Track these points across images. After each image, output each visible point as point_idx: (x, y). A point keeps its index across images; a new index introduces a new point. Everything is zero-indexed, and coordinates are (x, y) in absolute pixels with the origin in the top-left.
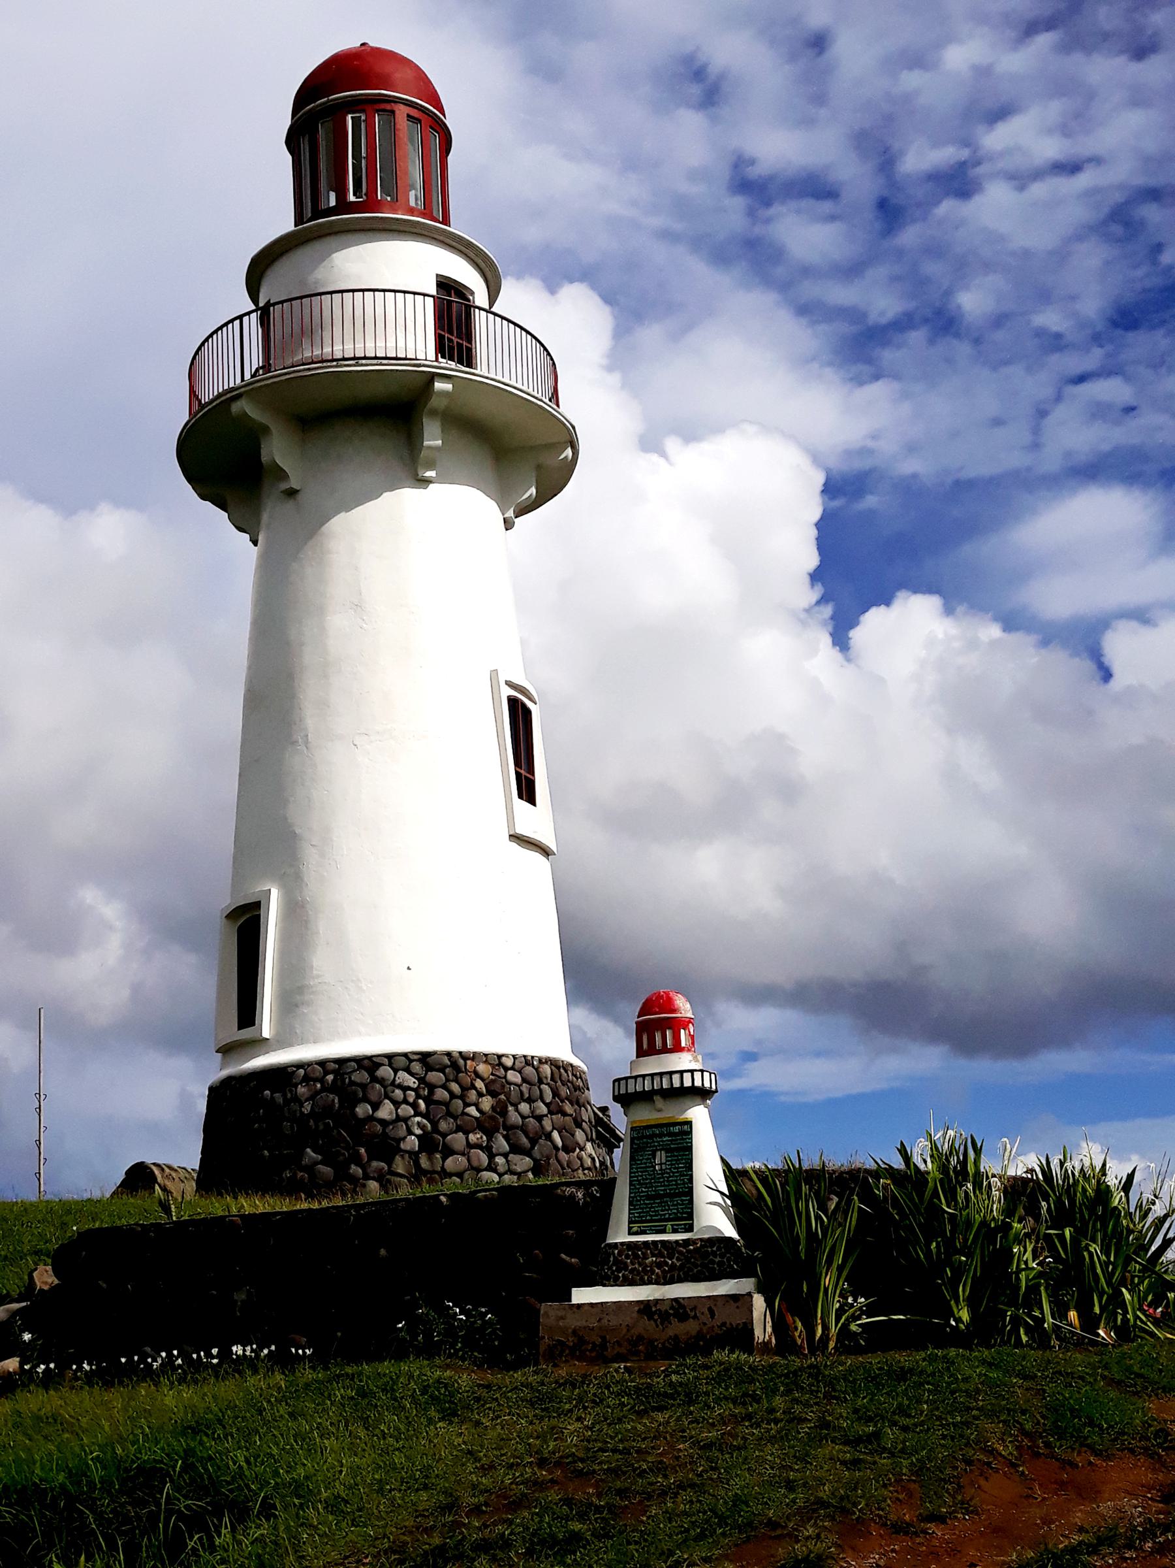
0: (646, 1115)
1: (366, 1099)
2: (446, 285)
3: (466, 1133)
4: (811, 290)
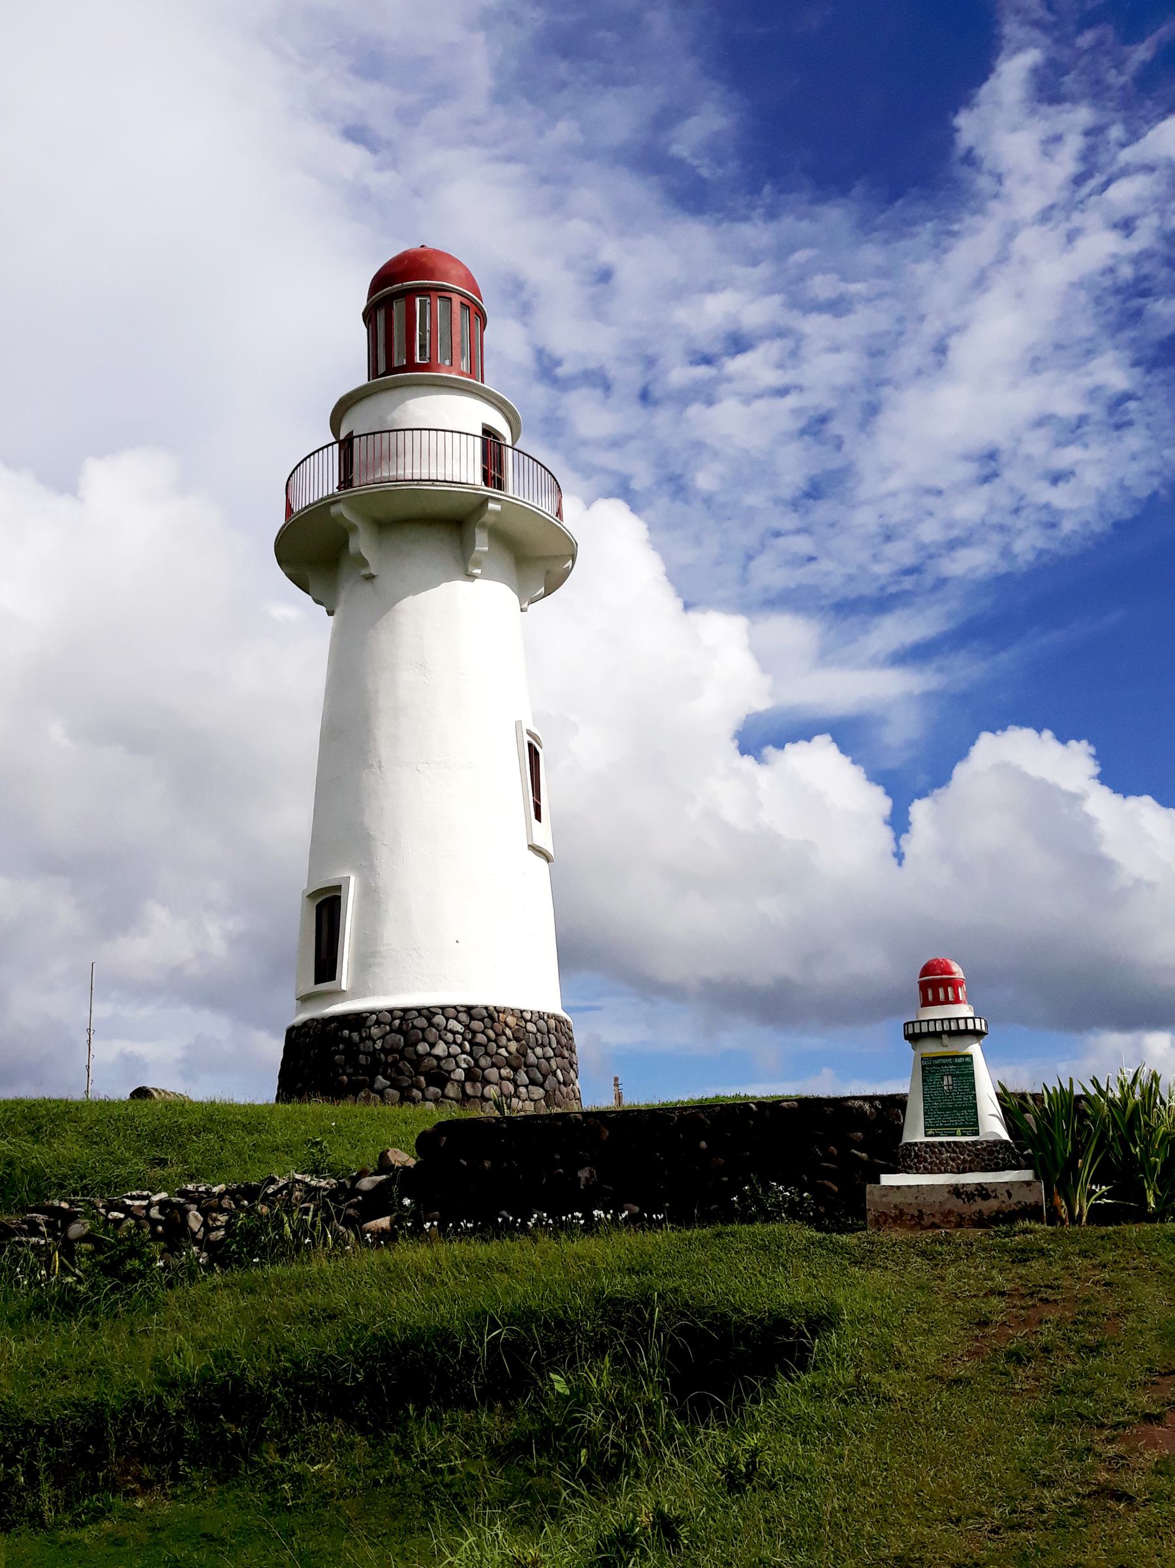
1: (424, 1040)
2: (489, 433)
3: (499, 1068)
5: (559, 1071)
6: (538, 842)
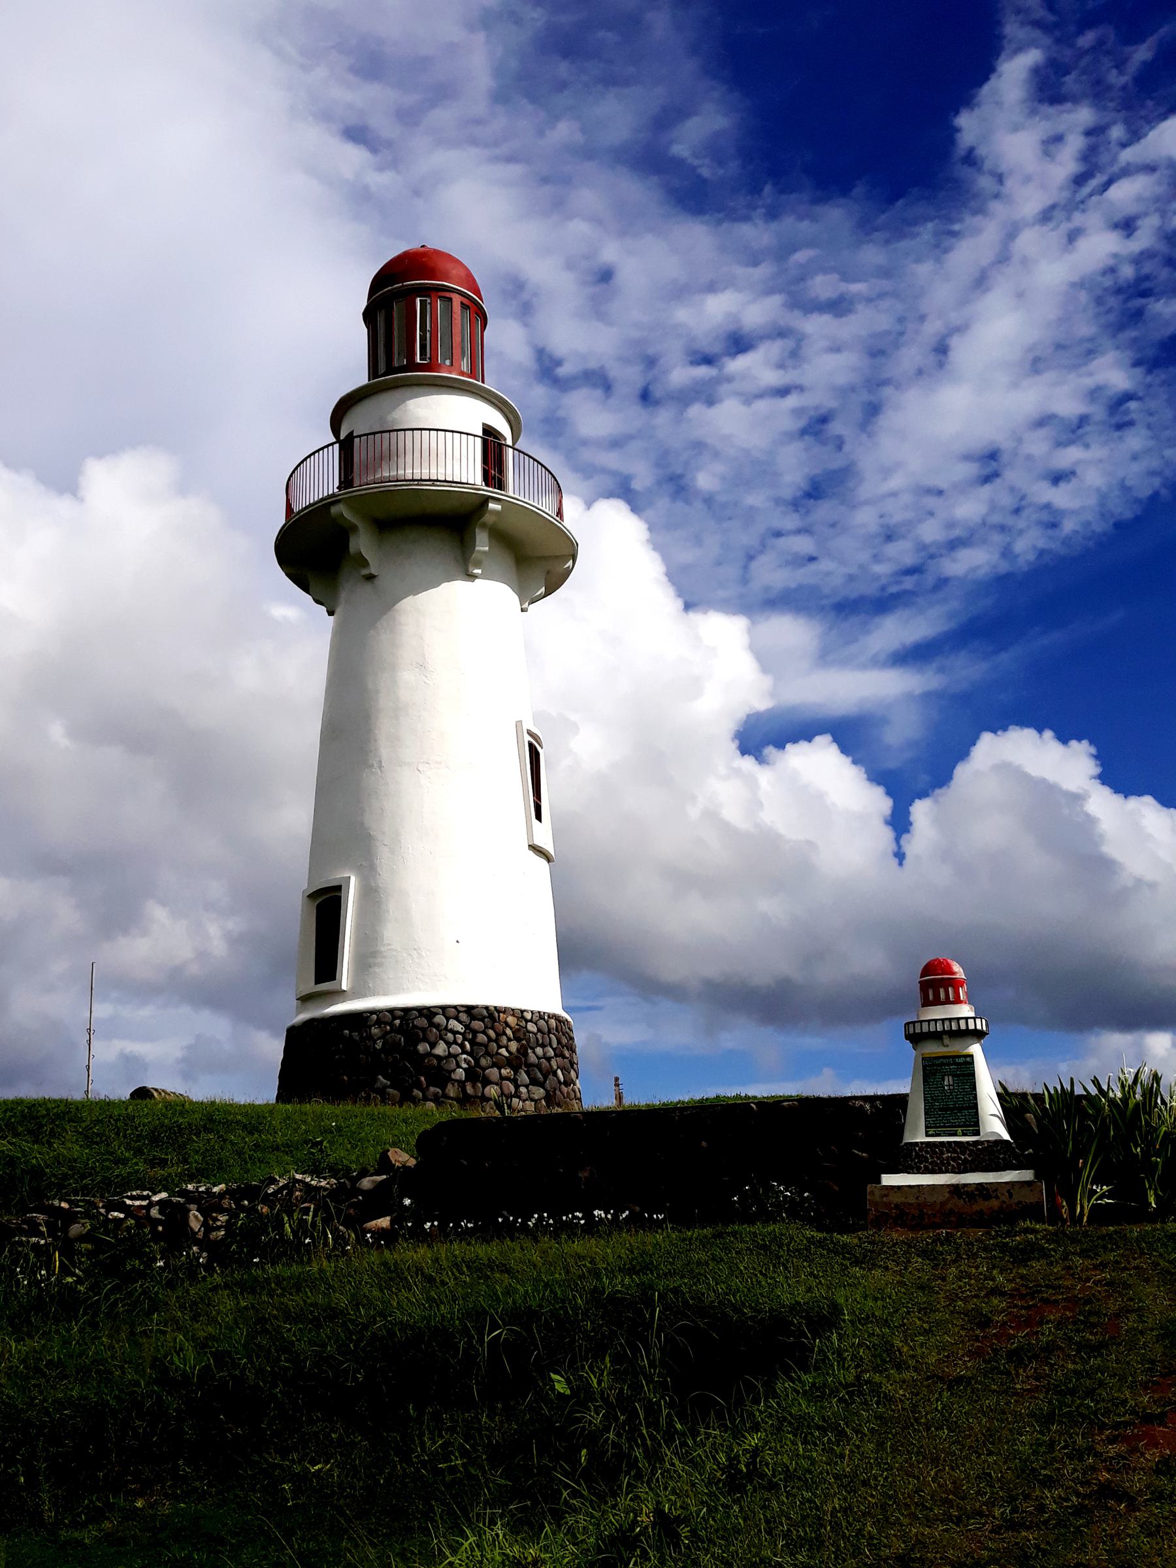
0: (933, 1049)
1: (425, 1040)
3: (499, 1069)
4: (587, 455)
5: (559, 1072)
6: (538, 842)
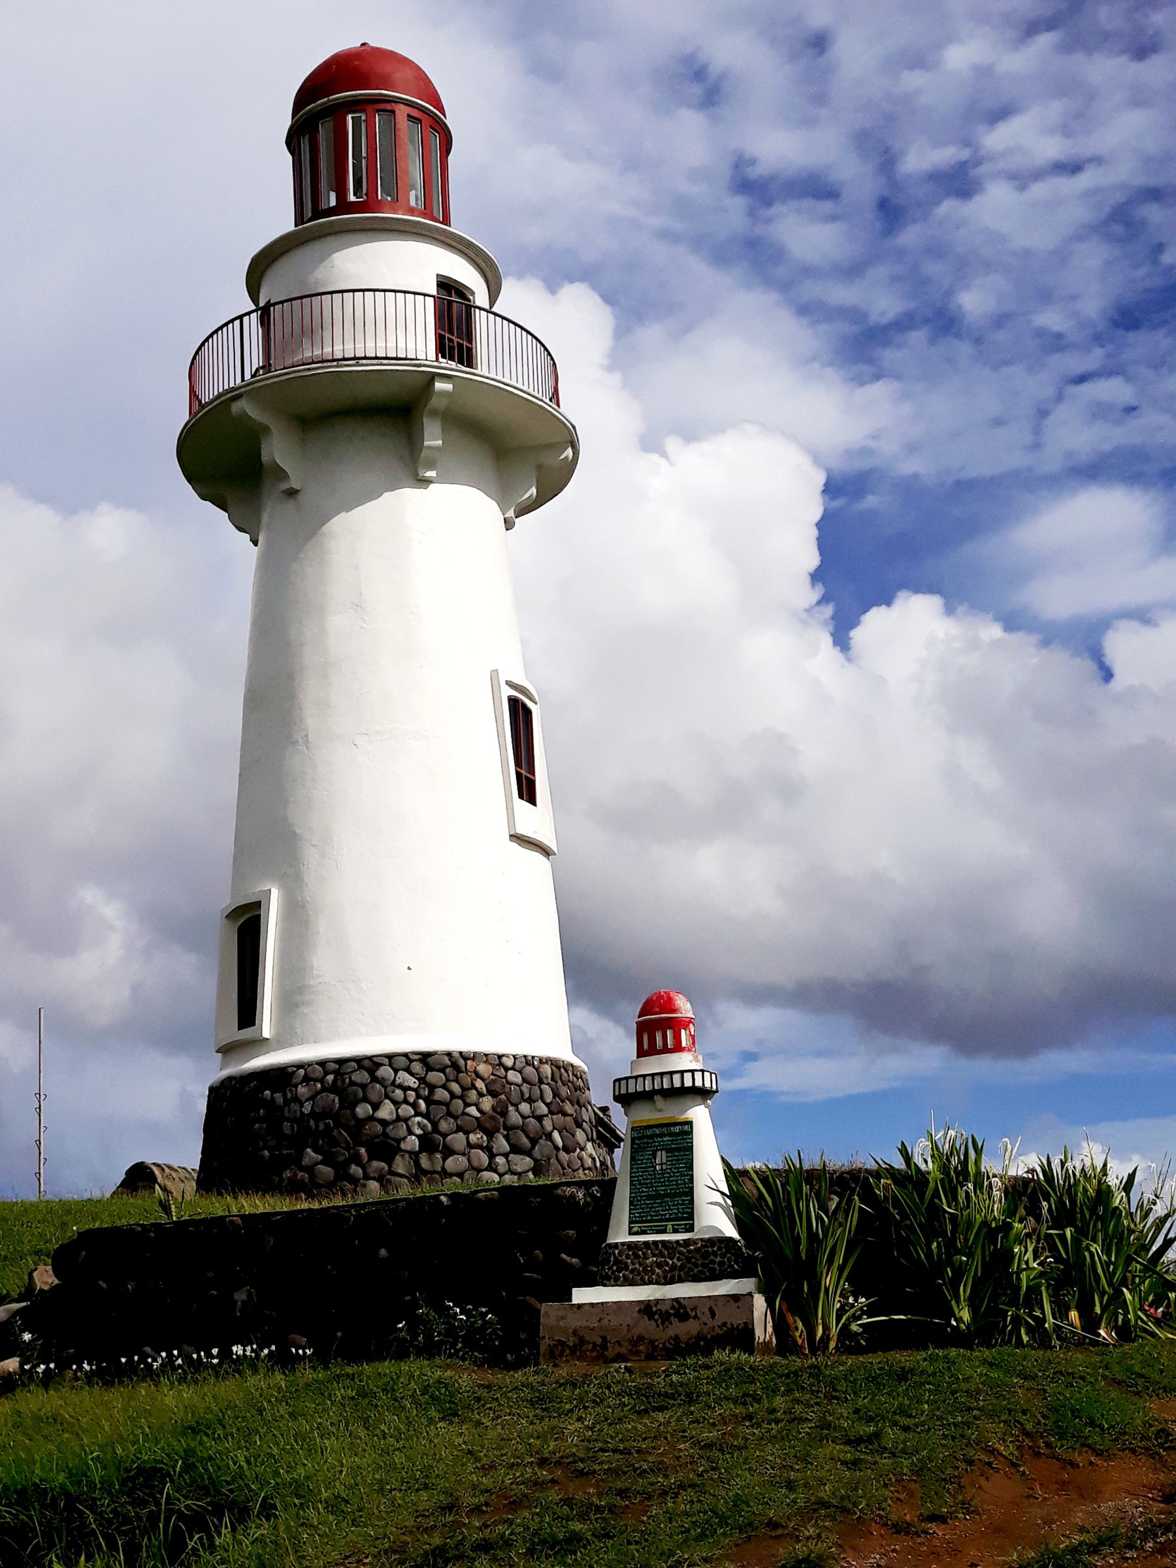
0: (646, 1114)
1: (365, 1099)
2: (446, 285)
3: (467, 1133)
4: (812, 290)
5: (556, 1135)
6: (521, 830)
